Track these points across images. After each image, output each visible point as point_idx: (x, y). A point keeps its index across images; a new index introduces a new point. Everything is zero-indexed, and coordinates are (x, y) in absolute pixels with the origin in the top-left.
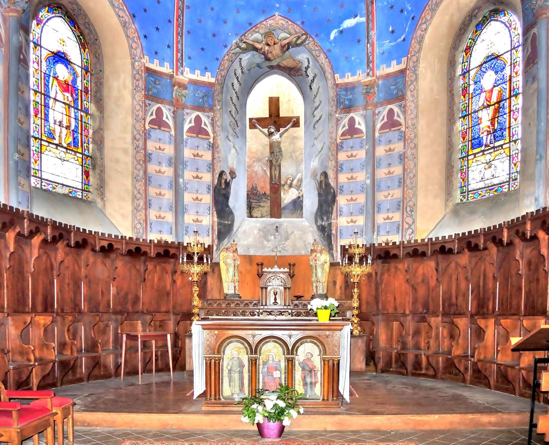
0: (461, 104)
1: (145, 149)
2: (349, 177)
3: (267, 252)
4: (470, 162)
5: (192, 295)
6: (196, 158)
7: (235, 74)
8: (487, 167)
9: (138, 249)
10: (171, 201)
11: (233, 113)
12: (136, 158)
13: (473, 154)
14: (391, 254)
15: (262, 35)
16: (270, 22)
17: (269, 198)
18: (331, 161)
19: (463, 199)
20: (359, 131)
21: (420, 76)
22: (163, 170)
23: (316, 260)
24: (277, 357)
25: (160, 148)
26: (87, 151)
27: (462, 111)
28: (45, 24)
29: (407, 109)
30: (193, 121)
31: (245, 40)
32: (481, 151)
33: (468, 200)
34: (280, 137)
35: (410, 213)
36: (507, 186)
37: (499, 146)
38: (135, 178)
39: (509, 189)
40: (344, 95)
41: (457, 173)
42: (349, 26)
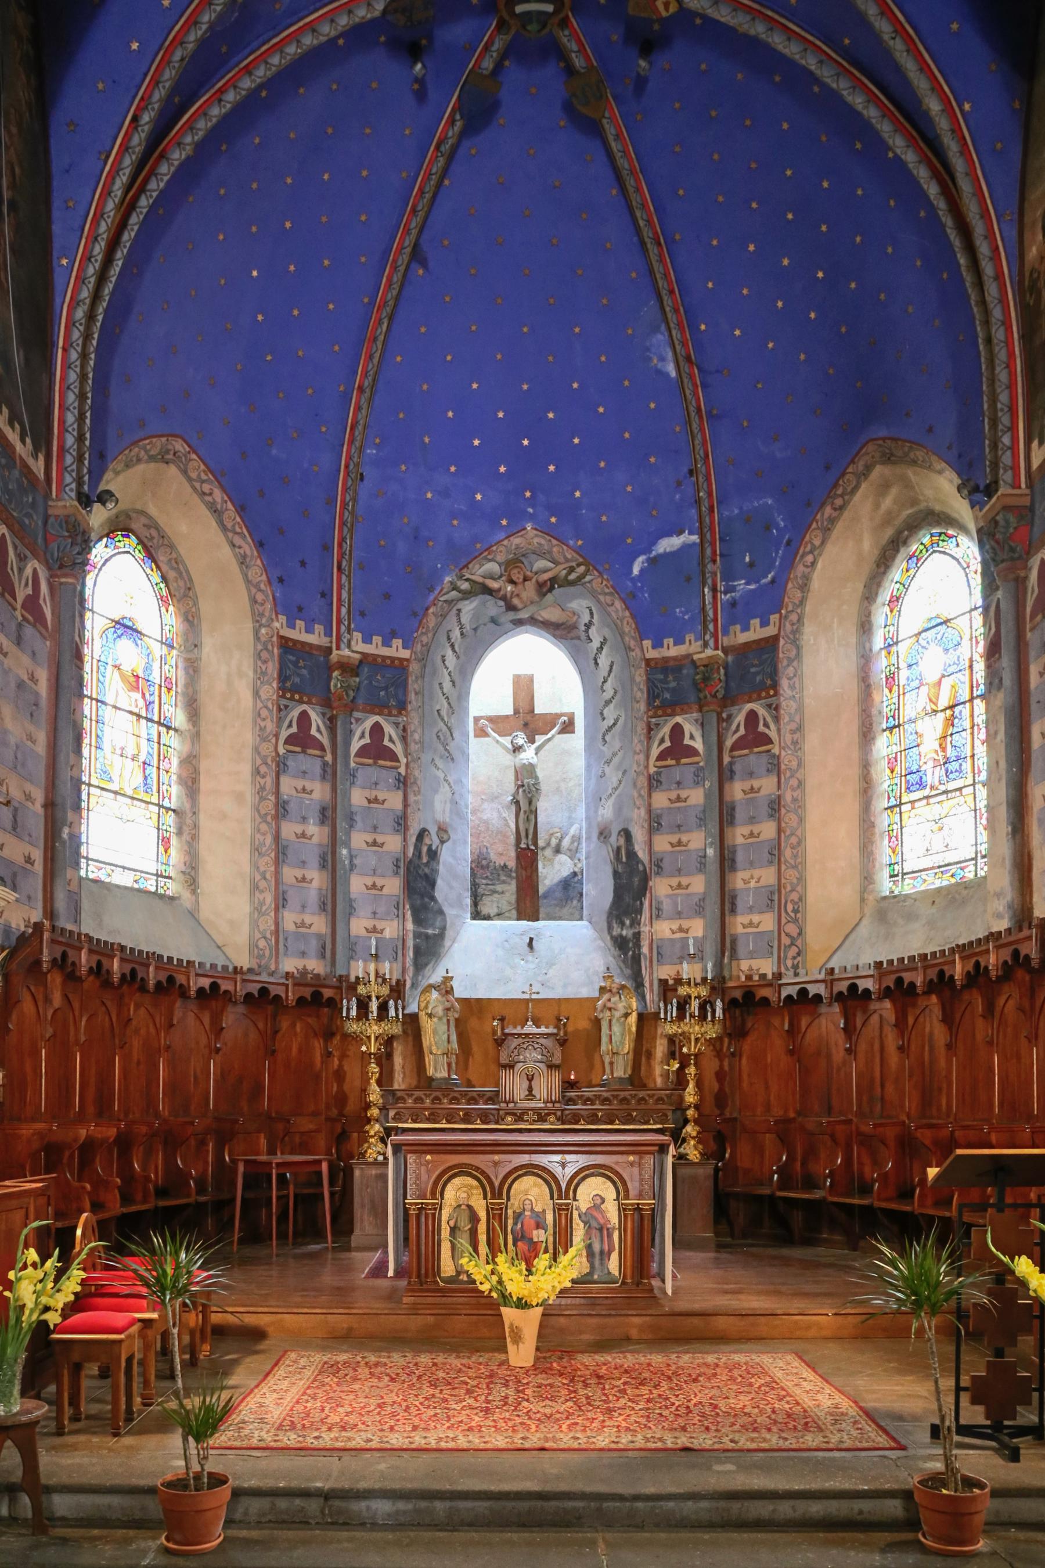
0: (885, 704)
1: (277, 792)
5: (367, 1081)
6: (372, 805)
7: (449, 638)
8: (936, 827)
9: (264, 991)
10: (324, 892)
11: (444, 713)
12: (258, 811)
14: (757, 998)
15: (500, 565)
16: (516, 541)
17: (514, 875)
18: (639, 808)
19: (894, 887)
20: (692, 752)
21: (805, 651)
22: (309, 833)
24: (539, 1204)
25: (304, 790)
26: (167, 800)
27: (888, 718)
28: (100, 569)
29: (782, 712)
30: (367, 735)
31: (468, 576)
35: (793, 915)
36: (972, 868)
38: (256, 850)
39: (976, 875)
40: (661, 681)
41: (882, 838)
42: (668, 550)
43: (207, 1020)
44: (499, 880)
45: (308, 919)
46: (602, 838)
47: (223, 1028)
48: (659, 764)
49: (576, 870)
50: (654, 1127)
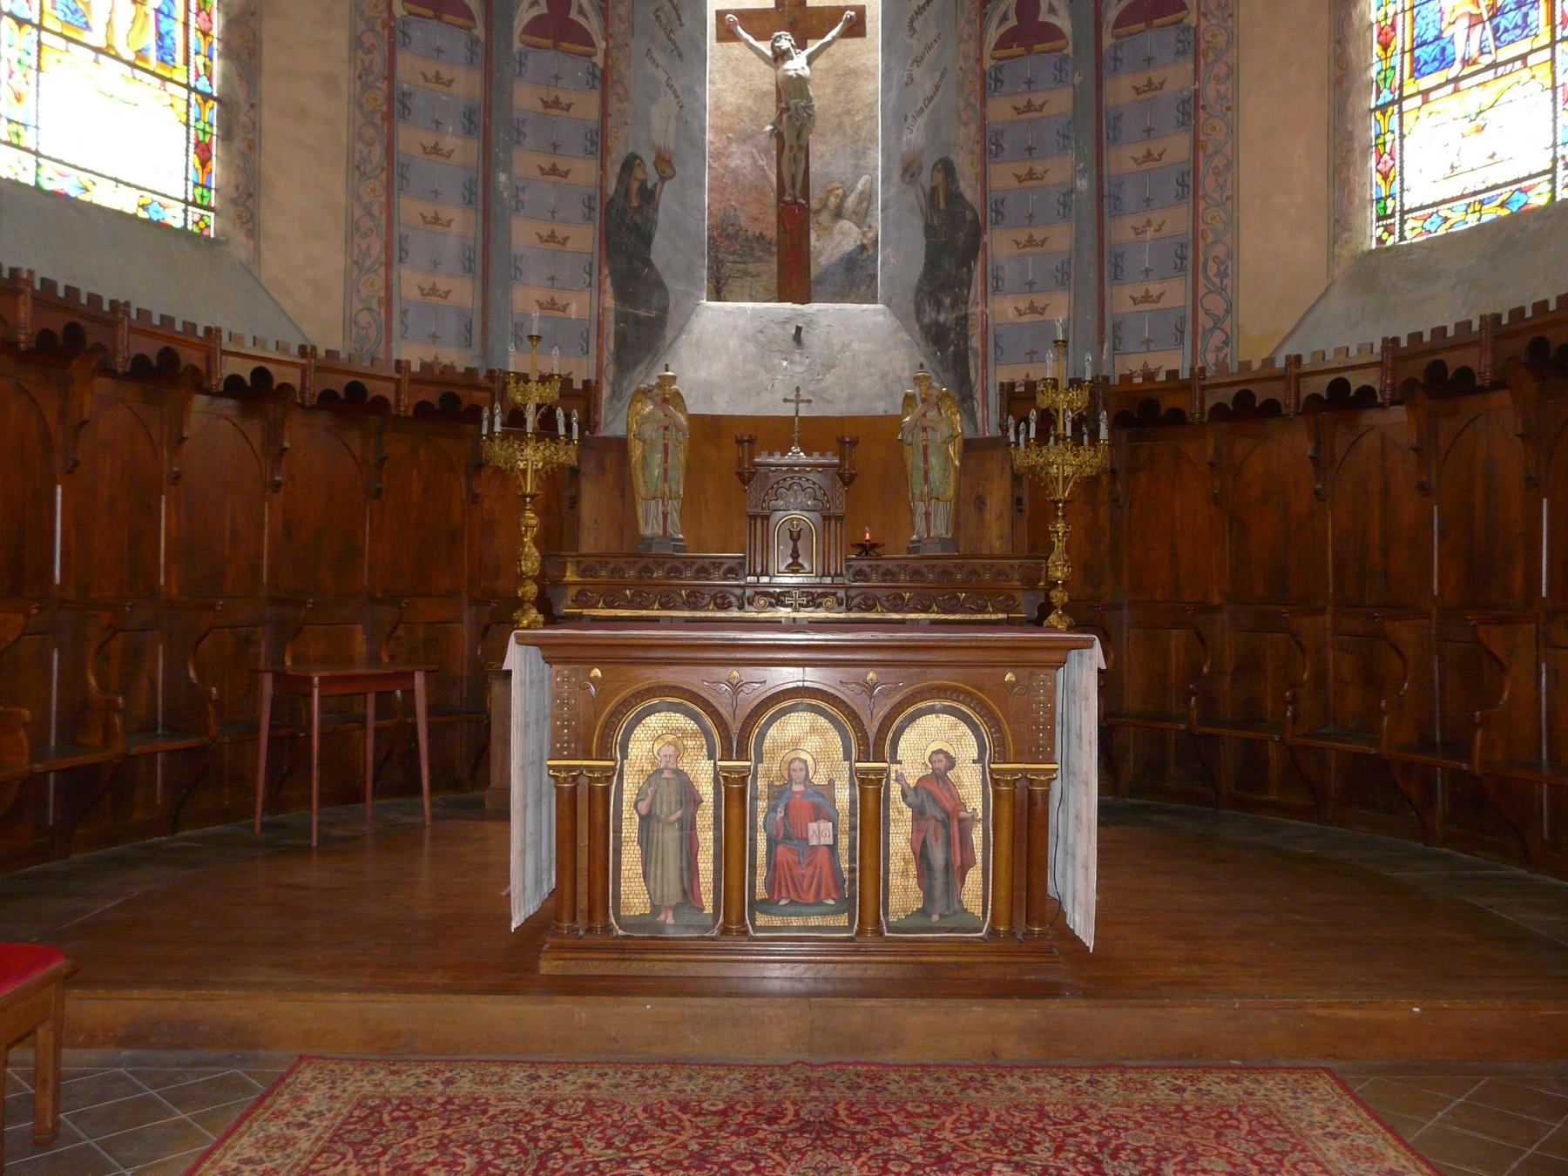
1: (390, 77)
2: (1023, 171)
3: (773, 404)
4: (1408, 119)
8: (1469, 127)
9: (355, 390)
12: (361, 106)
13: (1419, 93)
17: (775, 249)
18: (966, 125)
19: (1385, 236)
20: (1053, 33)
23: (924, 429)
24: (822, 769)
25: (438, 78)
26: (204, 80)
32: (1448, 82)
33: (1402, 238)
34: (809, 64)
35: (1217, 280)
37: (1513, 60)
38: (356, 168)
39: (1553, 197)
41: (1366, 158)
43: (256, 438)
44: (752, 256)
45: (443, 284)
46: (908, 178)
47: (284, 450)
48: (999, 53)
49: (865, 241)
50: (994, 617)
